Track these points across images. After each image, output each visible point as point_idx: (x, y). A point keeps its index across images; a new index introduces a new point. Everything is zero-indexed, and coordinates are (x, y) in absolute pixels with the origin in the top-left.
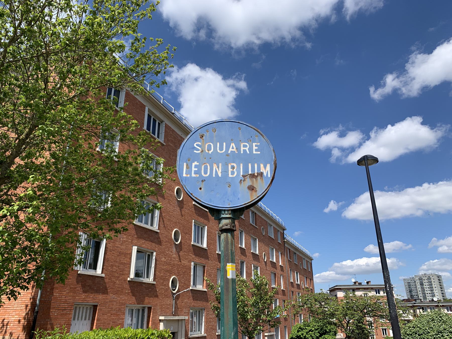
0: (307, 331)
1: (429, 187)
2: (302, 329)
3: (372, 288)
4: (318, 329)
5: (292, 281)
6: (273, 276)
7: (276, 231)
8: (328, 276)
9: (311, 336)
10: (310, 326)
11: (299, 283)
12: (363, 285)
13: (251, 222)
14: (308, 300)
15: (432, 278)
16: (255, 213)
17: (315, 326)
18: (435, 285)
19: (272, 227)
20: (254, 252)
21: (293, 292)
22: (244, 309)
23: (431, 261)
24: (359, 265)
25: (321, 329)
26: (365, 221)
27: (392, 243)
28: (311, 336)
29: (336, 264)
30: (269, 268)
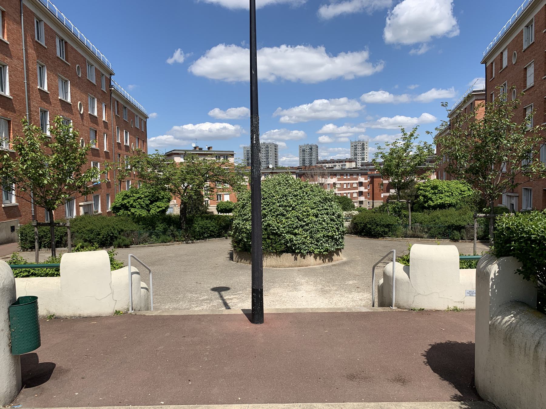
0: (135, 198)
1: (287, 50)
2: (129, 197)
3: (211, 154)
4: (149, 196)
5: (119, 141)
6: (92, 134)
7: (99, 75)
8: (165, 140)
9: (139, 204)
10: (139, 193)
11: (128, 144)
12: (205, 151)
13: (58, 54)
14: (138, 162)
15: (270, 147)
16: (66, 42)
17: (146, 192)
18: (271, 154)
20: (64, 100)
21: (120, 155)
22: (37, 172)
23: (272, 131)
24: (201, 130)
25: (153, 196)
26: (213, 80)
27: (239, 109)
28: (139, 204)
29: (176, 128)
30: (87, 122)
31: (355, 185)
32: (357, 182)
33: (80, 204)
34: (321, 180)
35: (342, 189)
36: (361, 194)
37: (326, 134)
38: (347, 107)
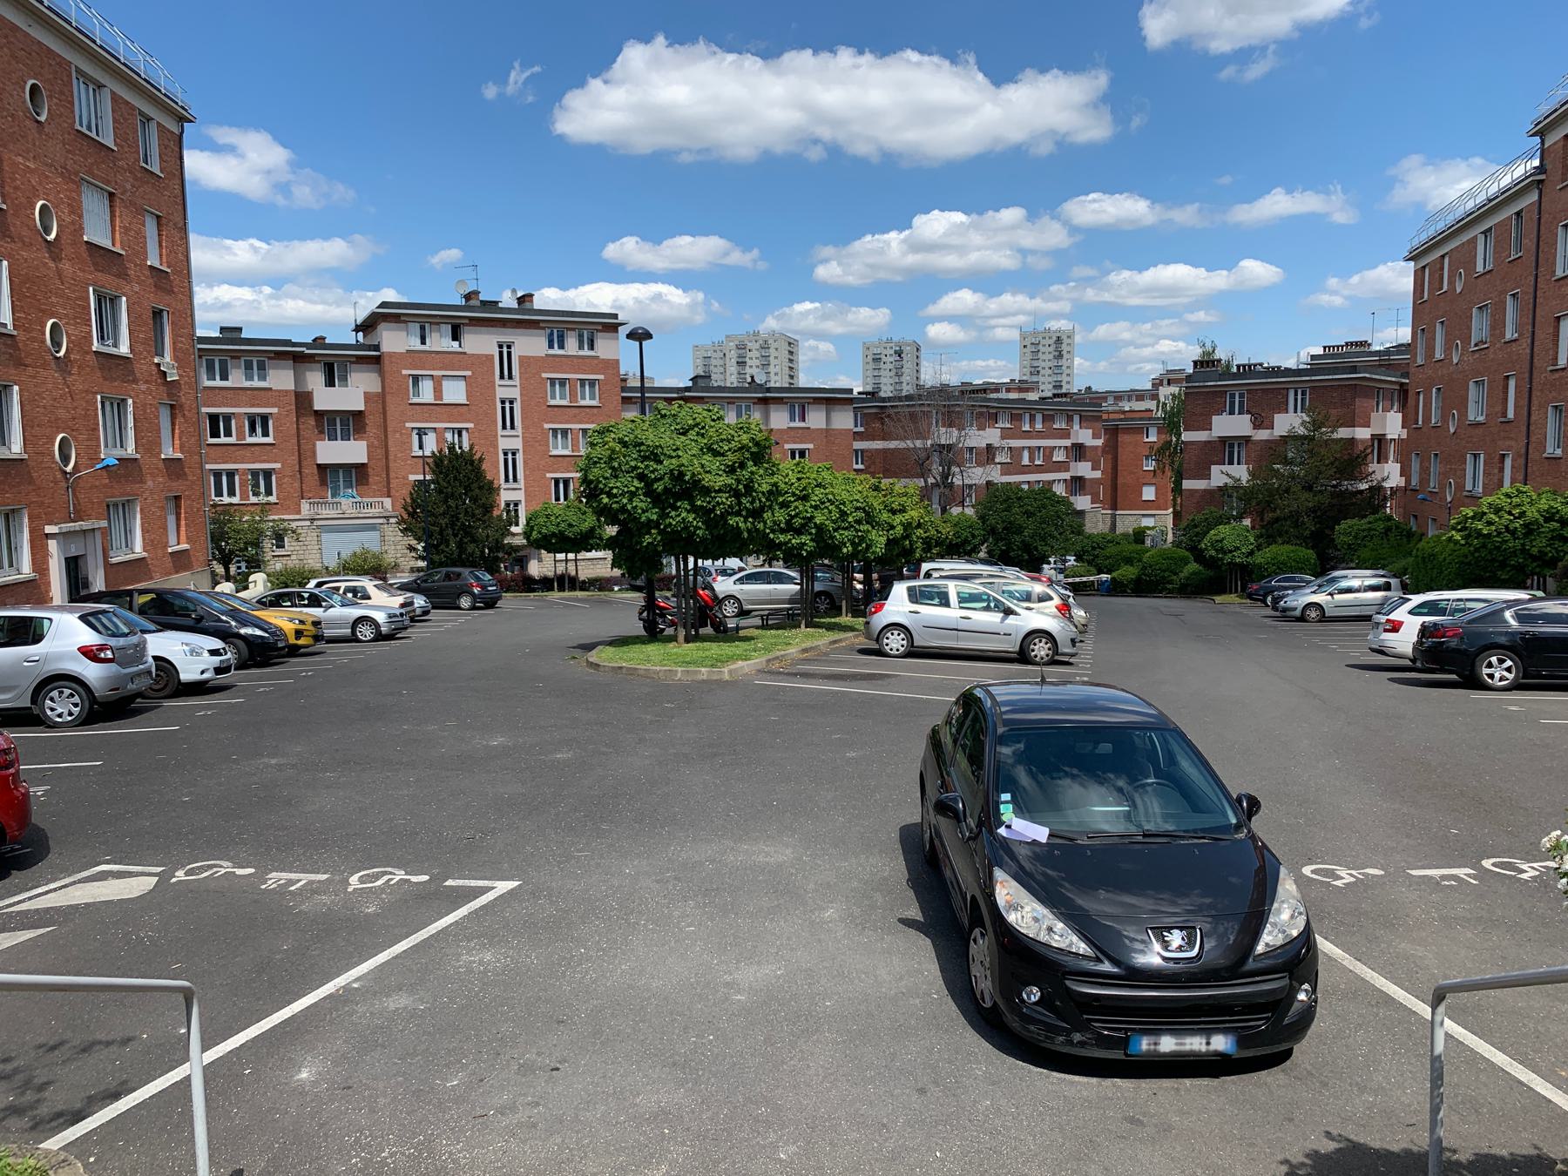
15: (773, 345)
19: (153, 126)
31: (1059, 457)
32: (1067, 443)
33: (49, 529)
34: (946, 436)
35: (1012, 467)
36: (1078, 484)
37: (951, 318)
38: (1028, 239)
